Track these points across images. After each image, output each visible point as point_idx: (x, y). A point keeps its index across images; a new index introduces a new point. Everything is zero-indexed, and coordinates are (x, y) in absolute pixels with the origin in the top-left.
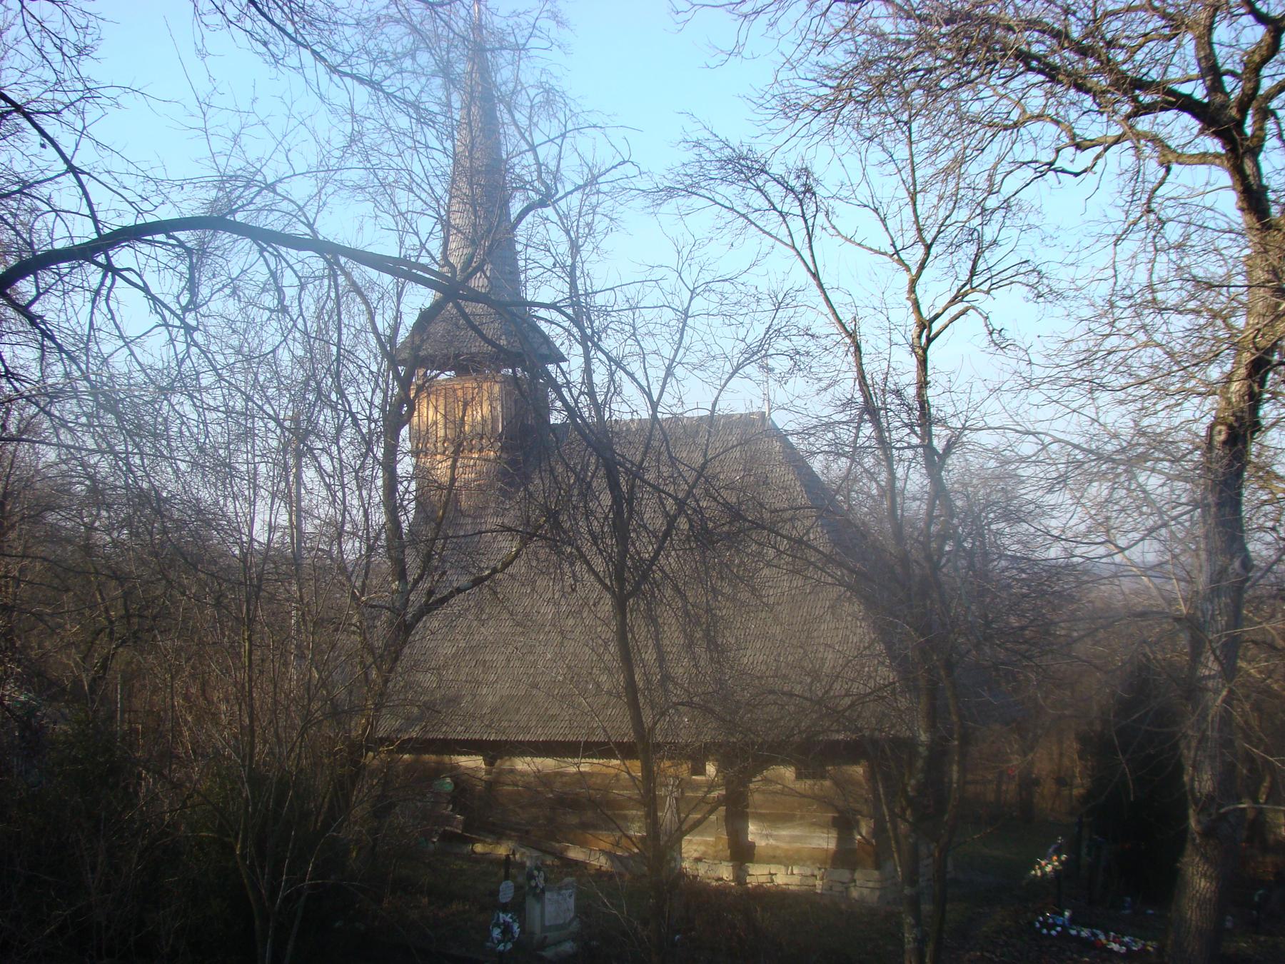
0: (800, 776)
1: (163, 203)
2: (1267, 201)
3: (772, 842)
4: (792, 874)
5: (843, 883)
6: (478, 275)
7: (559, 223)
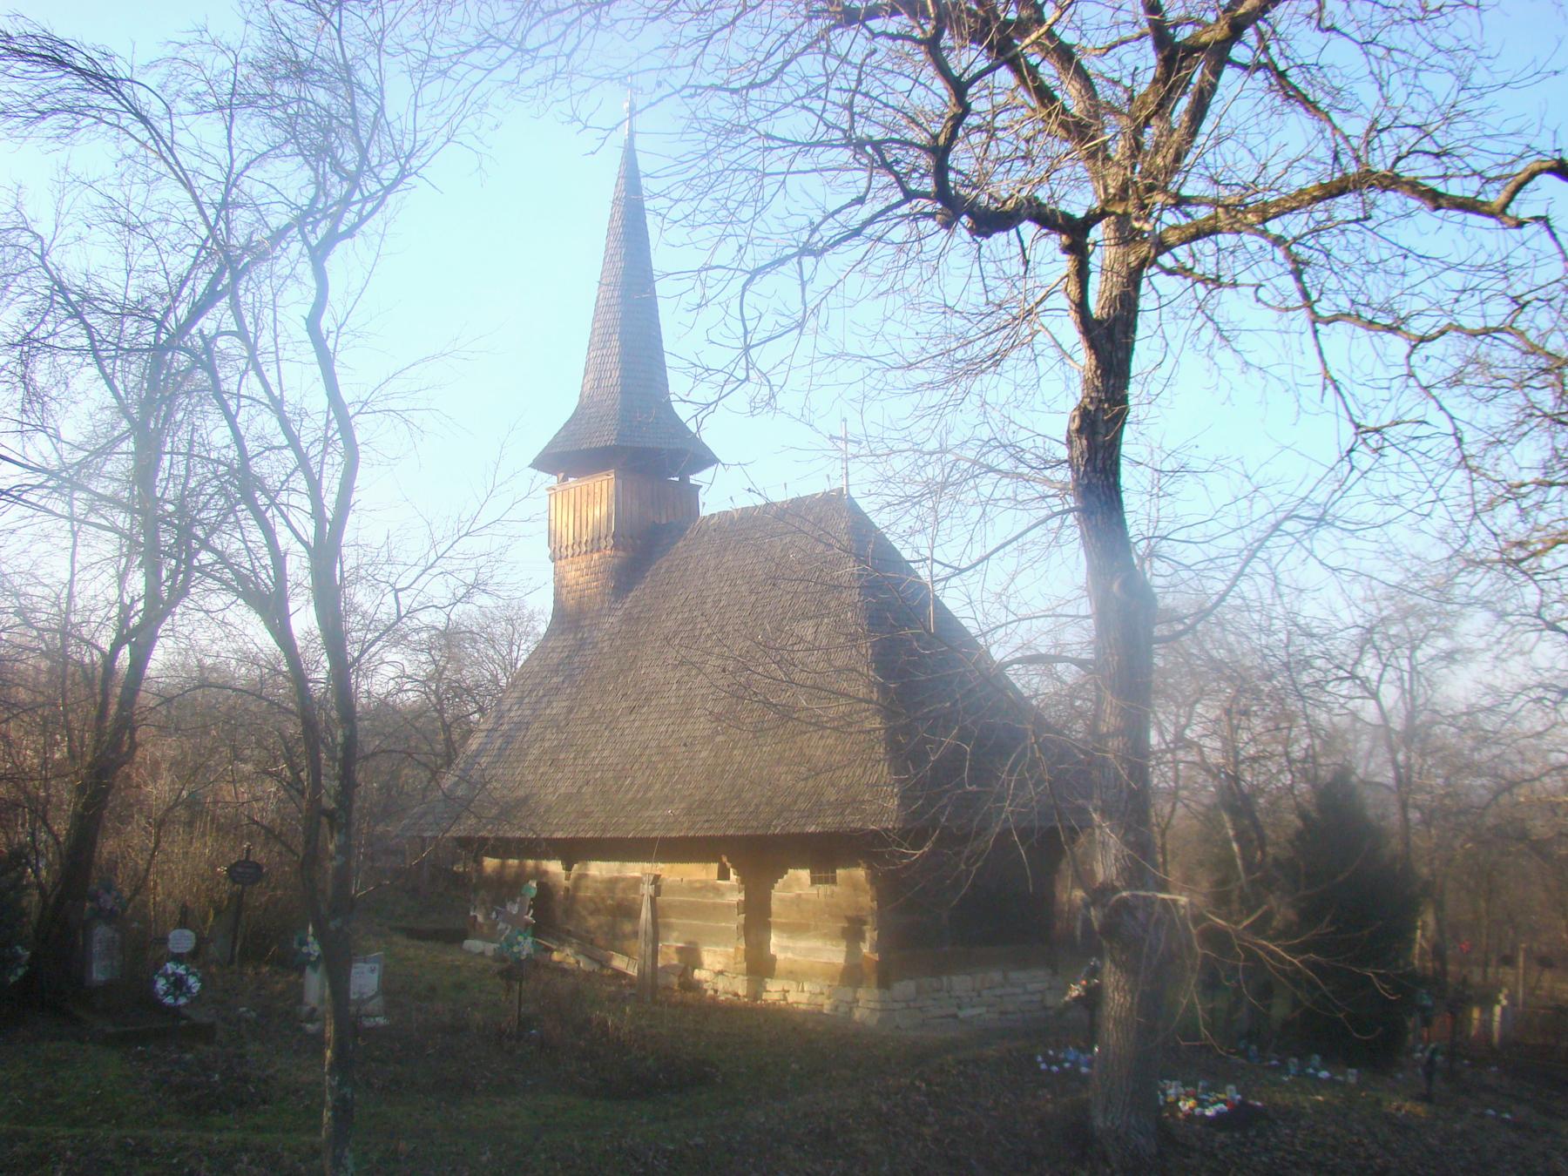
0: (814, 881)
2: (1331, 182)
3: (790, 955)
4: (803, 991)
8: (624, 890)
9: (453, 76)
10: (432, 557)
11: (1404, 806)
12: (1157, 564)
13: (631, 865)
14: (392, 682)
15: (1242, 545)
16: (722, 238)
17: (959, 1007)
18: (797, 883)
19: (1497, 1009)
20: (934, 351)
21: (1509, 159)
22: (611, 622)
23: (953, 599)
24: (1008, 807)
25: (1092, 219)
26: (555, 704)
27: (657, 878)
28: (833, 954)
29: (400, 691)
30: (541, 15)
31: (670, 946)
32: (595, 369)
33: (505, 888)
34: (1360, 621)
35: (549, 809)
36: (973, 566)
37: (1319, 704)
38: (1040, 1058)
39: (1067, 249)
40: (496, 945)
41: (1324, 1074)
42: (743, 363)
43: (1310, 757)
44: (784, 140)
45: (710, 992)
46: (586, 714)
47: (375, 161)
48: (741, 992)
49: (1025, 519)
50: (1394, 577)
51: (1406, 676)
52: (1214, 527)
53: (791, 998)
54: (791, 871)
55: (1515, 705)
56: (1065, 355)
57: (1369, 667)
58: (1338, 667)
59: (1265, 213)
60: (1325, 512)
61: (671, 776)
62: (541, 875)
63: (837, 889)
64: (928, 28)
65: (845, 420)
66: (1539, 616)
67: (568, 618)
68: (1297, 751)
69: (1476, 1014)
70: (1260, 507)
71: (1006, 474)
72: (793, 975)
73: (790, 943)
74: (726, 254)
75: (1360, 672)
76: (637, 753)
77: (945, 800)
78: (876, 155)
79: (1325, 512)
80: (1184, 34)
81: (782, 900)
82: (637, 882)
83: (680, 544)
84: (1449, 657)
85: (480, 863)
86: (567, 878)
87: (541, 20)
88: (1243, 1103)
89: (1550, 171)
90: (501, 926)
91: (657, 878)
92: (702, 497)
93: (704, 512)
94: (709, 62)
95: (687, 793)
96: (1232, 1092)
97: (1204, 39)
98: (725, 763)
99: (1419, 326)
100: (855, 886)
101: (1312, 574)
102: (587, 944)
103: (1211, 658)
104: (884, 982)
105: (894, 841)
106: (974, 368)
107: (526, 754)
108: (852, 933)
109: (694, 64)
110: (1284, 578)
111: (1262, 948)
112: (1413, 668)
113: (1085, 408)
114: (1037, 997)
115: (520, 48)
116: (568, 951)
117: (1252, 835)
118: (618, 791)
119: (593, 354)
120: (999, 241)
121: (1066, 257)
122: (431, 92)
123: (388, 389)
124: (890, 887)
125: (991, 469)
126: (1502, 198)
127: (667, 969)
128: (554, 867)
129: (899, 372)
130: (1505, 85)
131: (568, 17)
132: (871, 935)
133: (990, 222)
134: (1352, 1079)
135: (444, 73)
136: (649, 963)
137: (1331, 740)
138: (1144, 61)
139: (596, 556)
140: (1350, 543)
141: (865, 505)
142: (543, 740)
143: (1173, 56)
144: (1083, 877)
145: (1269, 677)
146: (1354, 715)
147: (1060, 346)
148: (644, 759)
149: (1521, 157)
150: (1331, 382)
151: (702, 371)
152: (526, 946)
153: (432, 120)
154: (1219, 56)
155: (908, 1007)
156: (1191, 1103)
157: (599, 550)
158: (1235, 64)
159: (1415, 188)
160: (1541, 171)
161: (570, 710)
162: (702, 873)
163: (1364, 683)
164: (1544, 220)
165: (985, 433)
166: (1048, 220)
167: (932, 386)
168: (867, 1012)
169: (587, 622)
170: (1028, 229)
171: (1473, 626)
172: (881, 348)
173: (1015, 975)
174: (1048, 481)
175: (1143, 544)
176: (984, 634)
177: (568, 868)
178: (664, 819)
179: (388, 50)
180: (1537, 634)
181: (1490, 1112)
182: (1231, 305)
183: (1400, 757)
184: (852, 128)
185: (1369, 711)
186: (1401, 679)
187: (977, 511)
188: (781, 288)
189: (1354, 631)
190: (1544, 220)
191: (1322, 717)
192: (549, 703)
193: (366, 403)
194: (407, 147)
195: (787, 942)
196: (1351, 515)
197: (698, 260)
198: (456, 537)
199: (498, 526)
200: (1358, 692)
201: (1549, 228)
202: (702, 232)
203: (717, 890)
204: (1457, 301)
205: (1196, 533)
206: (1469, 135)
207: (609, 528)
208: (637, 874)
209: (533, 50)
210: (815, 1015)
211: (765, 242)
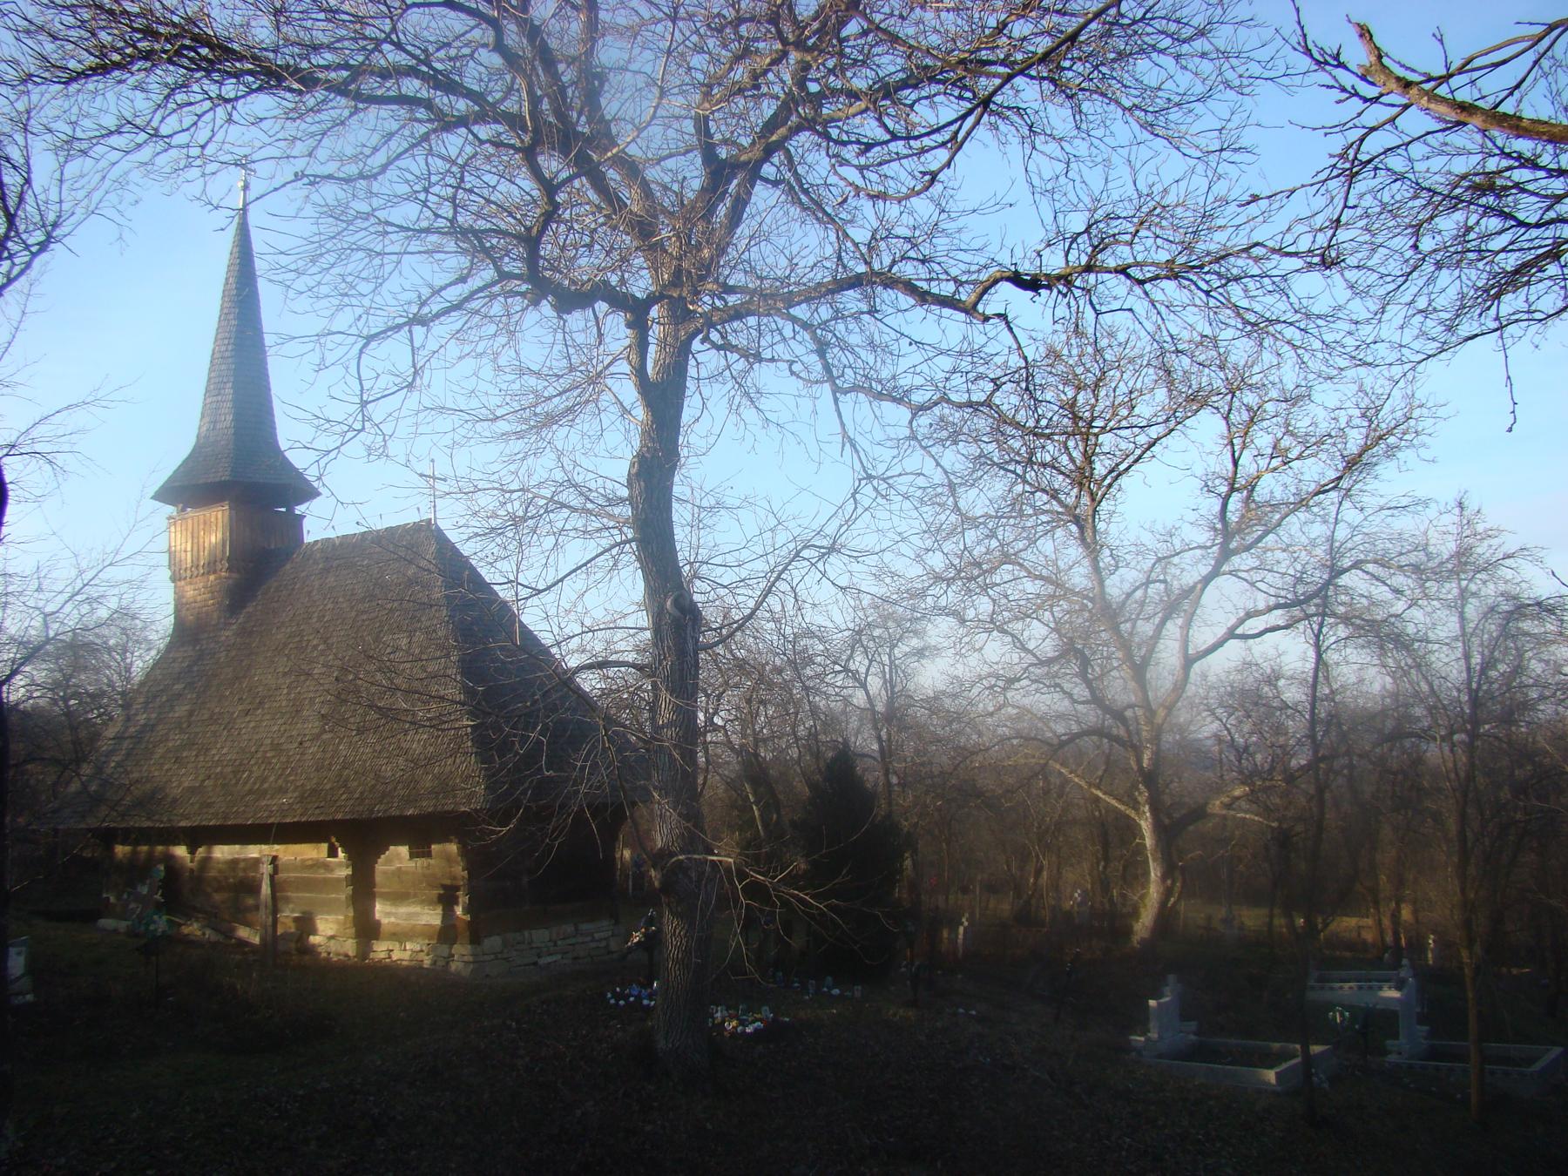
0: (412, 856)
3: (393, 920)
8: (244, 870)
9: (93, 155)
10: (79, 584)
11: (887, 774)
12: (698, 583)
13: (251, 847)
14: (22, 690)
15: (767, 568)
16: (340, 308)
17: (539, 957)
18: (398, 858)
19: (961, 929)
20: (516, 406)
21: (974, 268)
22: (227, 634)
23: (531, 617)
24: (583, 789)
25: (652, 300)
26: (177, 708)
27: (275, 859)
28: (432, 917)
29: (31, 698)
30: (174, 106)
31: (288, 915)
32: (210, 412)
33: (136, 871)
34: (851, 626)
35: (175, 801)
36: (548, 588)
37: (818, 692)
38: (609, 995)
39: (629, 325)
40: (129, 923)
41: (836, 991)
42: (360, 417)
43: (813, 735)
44: (397, 226)
45: (324, 955)
46: (206, 717)
47: (22, 228)
48: (351, 953)
49: (592, 547)
50: (881, 591)
51: (887, 669)
52: (745, 555)
53: (395, 956)
54: (392, 848)
55: (975, 691)
56: (625, 412)
57: (859, 663)
58: (835, 663)
59: (790, 301)
60: (834, 542)
61: (284, 769)
62: (169, 859)
63: (432, 862)
64: (527, 139)
65: (433, 461)
66: (992, 621)
67: (188, 631)
68: (802, 731)
69: (945, 934)
70: (782, 538)
71: (574, 510)
72: (400, 936)
73: (393, 910)
74: (343, 320)
75: (852, 667)
76: (253, 749)
77: (526, 785)
78: (474, 241)
79: (834, 542)
80: (723, 153)
81: (385, 873)
82: (257, 862)
83: (288, 566)
84: (920, 653)
85: (112, 849)
86: (192, 861)
87: (175, 111)
88: (774, 1020)
89: (1008, 279)
90: (132, 905)
91: (275, 859)
92: (307, 524)
93: (308, 539)
94: (322, 154)
95: (298, 784)
96: (767, 1012)
97: (744, 158)
98: (333, 757)
99: (918, 398)
100: (448, 859)
101: (826, 592)
102: (212, 918)
103: (735, 658)
104: (475, 939)
105: (484, 820)
106: (551, 420)
107: (152, 753)
108: (447, 899)
109: (310, 155)
110: (802, 594)
111: (793, 896)
112: (891, 662)
113: (643, 456)
114: (603, 944)
115: (156, 134)
116: (196, 925)
117: (770, 802)
118: (237, 783)
119: (209, 400)
120: (577, 319)
121: (629, 331)
122: (72, 168)
123: (35, 433)
124: (476, 860)
125: (563, 506)
126: (973, 297)
127: (285, 936)
128: (181, 851)
129: (486, 424)
130: (974, 211)
131: (198, 109)
132: (463, 899)
133: (570, 300)
134: (858, 994)
135: (84, 153)
136: (270, 930)
137: (831, 722)
138: (693, 173)
139: (212, 577)
140: (855, 567)
141: (452, 536)
142: (167, 740)
143: (719, 172)
144: (640, 840)
145: (779, 671)
146: (846, 701)
147: (621, 404)
148: (259, 755)
149: (985, 267)
150: (849, 441)
151: (323, 423)
152: (161, 923)
153: (73, 193)
154: (753, 174)
155: (497, 959)
156: (734, 1023)
157: (215, 572)
158: (766, 180)
159: (909, 287)
160: (1002, 279)
161: (191, 713)
162: (314, 852)
163: (855, 675)
164: (1002, 317)
165: (559, 476)
166: (619, 301)
167: (519, 435)
168: (460, 965)
169: (206, 635)
170: (602, 307)
171: (940, 630)
172: (474, 403)
173: (584, 927)
174: (611, 516)
175: (687, 568)
176: (558, 644)
177: (192, 852)
178: (281, 806)
179: (34, 131)
180: (986, 635)
181: (961, 1010)
182: (764, 375)
183: (884, 734)
184: (455, 217)
185: (859, 698)
186: (884, 672)
187: (552, 540)
188: (394, 353)
189: (847, 633)
190: (1002, 317)
191: (821, 703)
192: (172, 707)
193: (13, 446)
194: (51, 217)
195: (388, 908)
196: (851, 545)
197: (318, 325)
198: (100, 567)
199: (139, 557)
200: (850, 683)
201: (1008, 324)
202: (324, 303)
203: (326, 867)
204: (947, 379)
205: (730, 559)
206: (946, 248)
207: (224, 551)
208: (255, 855)
209: (167, 137)
210: (415, 970)
211: (379, 312)
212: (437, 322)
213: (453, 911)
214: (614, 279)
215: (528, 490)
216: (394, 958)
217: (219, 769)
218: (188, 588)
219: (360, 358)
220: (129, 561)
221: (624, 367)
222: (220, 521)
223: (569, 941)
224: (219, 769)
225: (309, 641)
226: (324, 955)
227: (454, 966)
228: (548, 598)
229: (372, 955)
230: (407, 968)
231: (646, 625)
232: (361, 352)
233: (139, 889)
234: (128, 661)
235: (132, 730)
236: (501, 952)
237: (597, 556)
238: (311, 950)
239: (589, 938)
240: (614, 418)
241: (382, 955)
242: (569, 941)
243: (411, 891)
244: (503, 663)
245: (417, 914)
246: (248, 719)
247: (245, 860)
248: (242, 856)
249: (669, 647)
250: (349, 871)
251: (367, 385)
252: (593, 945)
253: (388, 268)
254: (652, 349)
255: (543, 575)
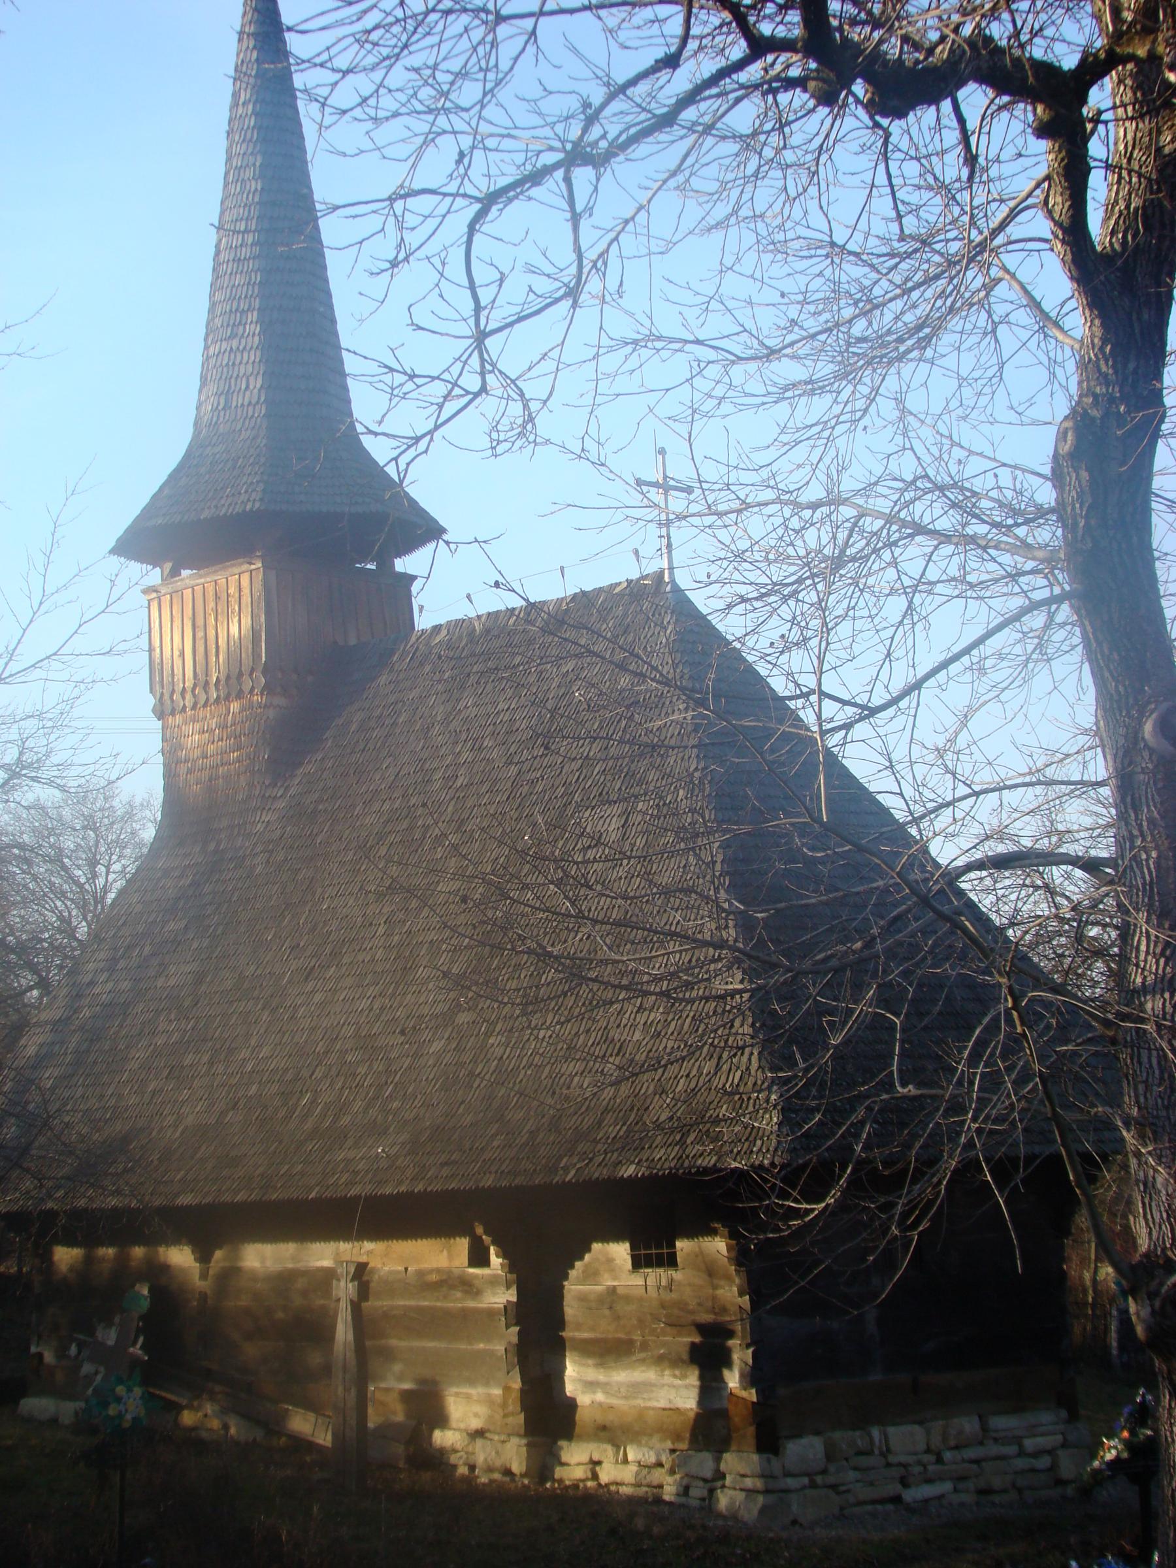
0: (638, 1263)
1: (996, 476)
3: (600, 1397)
4: (625, 1461)
5: (705, 1480)
6: (963, 886)
7: (922, 289)
8: (305, 1293)
16: (430, 139)
17: (904, 1482)
20: (812, 325)
39: (1043, 131)
40: (80, 1404)
49: (980, 616)
53: (607, 1474)
54: (596, 1246)
56: (1047, 322)
62: (158, 1273)
63: (677, 1275)
65: (662, 452)
71: (944, 537)
73: (601, 1377)
76: (320, 1048)
77: (861, 1112)
81: (582, 1298)
82: (329, 1275)
83: (383, 679)
86: (204, 1276)
90: (87, 1368)
93: (423, 622)
100: (710, 1271)
114: (1044, 1462)
116: (209, 1408)
121: (1043, 145)
125: (919, 529)
127: (387, 1431)
128: (180, 1257)
129: (752, 366)
132: (741, 1355)
136: (353, 1422)
139: (235, 706)
141: (703, 601)
155: (813, 1485)
165: (907, 468)
167: (812, 387)
168: (740, 1496)
173: (1002, 1423)
174: (1025, 547)
177: (204, 1257)
195: (593, 1373)
199: (56, 665)
203: (468, 1287)
207: (256, 655)
208: (327, 1263)
212: (621, 158)
213: (721, 1380)
214: (999, 31)
215: (845, 501)
216: (604, 1478)
217: (254, 1089)
218: (188, 729)
219: (469, 243)
220: (38, 673)
221: (1036, 224)
222: (246, 591)
223: (970, 1453)
224: (254, 1089)
225: (426, 828)
226: (463, 1470)
227: (724, 1500)
228: (890, 723)
229: (559, 1472)
230: (630, 1499)
231: (1102, 774)
232: (472, 229)
233: (100, 1334)
234: (101, 881)
235: (86, 1013)
236: (824, 1472)
237: (989, 634)
238: (437, 1461)
239: (1011, 1450)
240: (1024, 335)
241: (579, 1473)
242: (970, 1453)
243: (637, 1337)
244: (811, 862)
245: (648, 1386)
246: (310, 986)
247: (306, 1273)
248: (300, 1266)
249: (1151, 821)
250: (511, 1296)
251: (485, 296)
252: (1021, 1463)
253: (507, 51)
254: (1099, 187)
255: (884, 676)
